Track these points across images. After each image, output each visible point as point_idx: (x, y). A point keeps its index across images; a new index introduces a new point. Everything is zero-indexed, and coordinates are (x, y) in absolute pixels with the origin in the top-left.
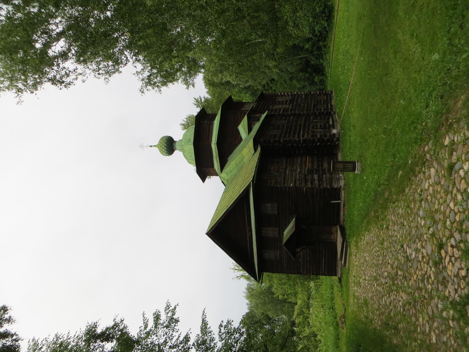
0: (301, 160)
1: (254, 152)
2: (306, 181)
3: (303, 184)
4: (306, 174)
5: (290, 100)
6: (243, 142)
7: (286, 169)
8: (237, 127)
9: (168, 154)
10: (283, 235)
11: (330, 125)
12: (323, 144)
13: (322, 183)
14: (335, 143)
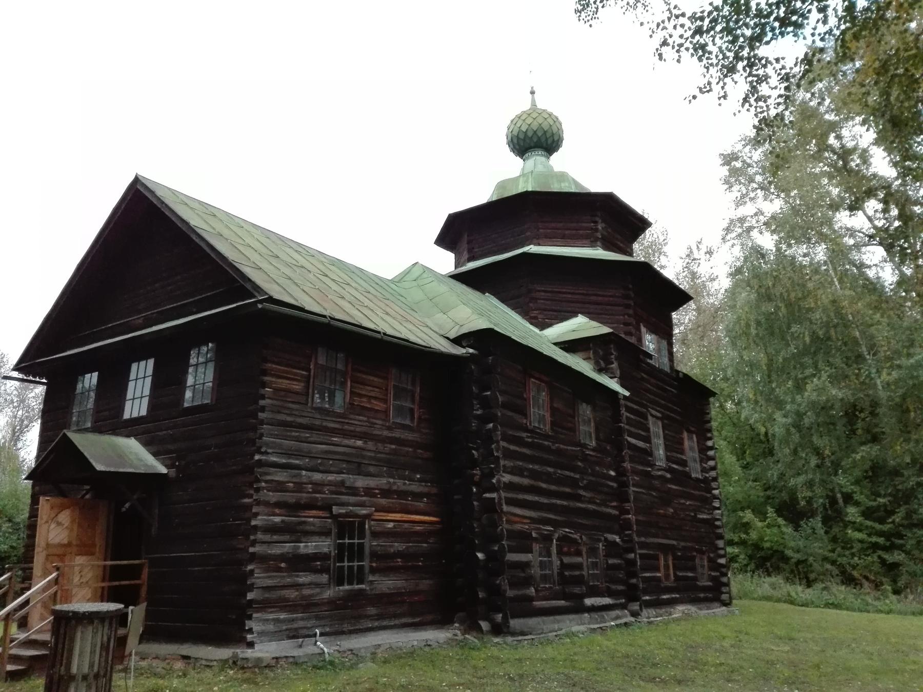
0: (417, 496)
1: (451, 338)
2: (294, 508)
3: (273, 497)
4: (335, 510)
5: (687, 475)
6: (536, 330)
8: (582, 313)
9: (510, 138)
10: (128, 436)
11: (582, 596)
13: (279, 570)
14: (485, 619)
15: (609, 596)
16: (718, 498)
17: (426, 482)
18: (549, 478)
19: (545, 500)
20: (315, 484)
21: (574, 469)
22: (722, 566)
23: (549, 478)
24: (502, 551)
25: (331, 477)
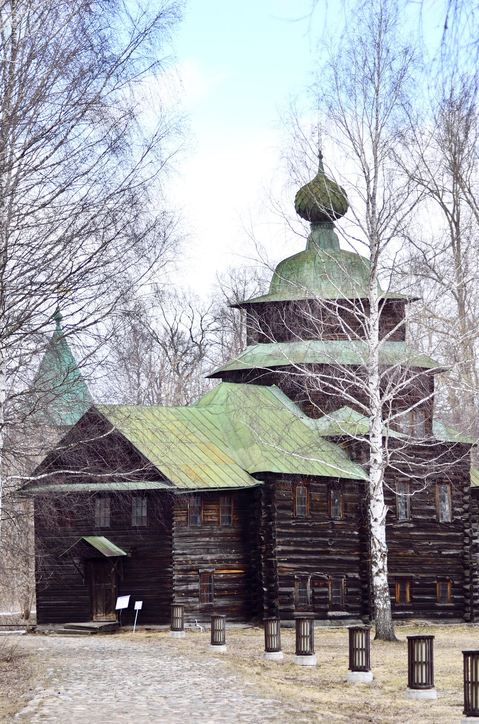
0: (233, 561)
2: (185, 571)
3: (179, 567)
4: (200, 571)
7: (209, 535)
11: (327, 610)
12: (265, 598)
13: (182, 596)
15: (347, 611)
16: (468, 536)
17: (227, 547)
18: (307, 544)
19: (304, 557)
20: (192, 560)
21: (325, 535)
22: (467, 590)
23: (307, 544)
24: (276, 587)
25: (198, 557)
